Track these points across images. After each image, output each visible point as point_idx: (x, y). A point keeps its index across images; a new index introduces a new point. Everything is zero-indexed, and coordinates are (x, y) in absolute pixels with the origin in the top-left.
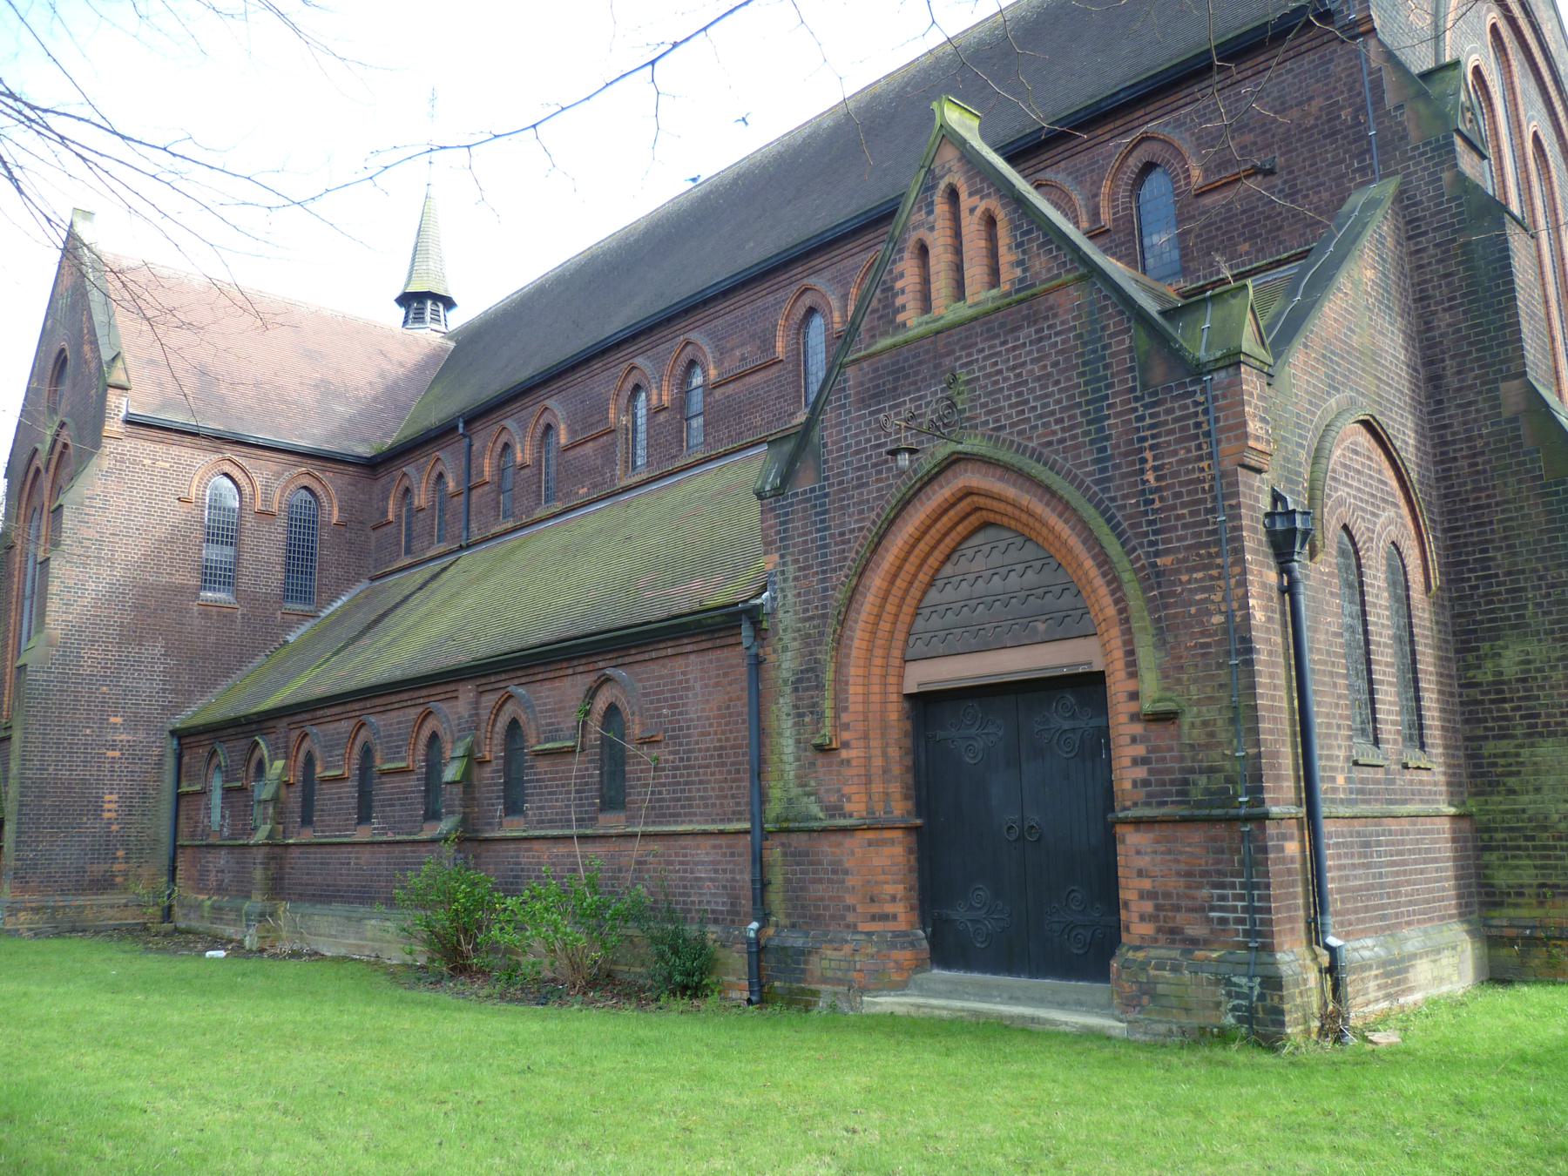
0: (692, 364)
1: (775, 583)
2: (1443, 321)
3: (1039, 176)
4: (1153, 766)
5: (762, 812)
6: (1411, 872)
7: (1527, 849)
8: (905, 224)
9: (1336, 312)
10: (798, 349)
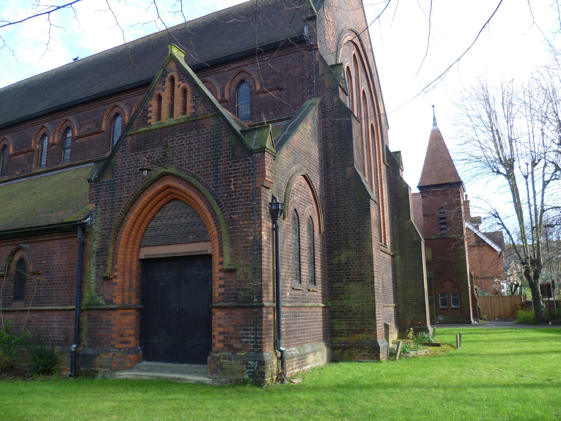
0: (68, 128)
1: (92, 215)
2: (331, 145)
3: (205, 78)
4: (227, 288)
5: (81, 302)
6: (309, 326)
7: (345, 318)
8: (154, 88)
9: (298, 138)
10: (111, 128)
